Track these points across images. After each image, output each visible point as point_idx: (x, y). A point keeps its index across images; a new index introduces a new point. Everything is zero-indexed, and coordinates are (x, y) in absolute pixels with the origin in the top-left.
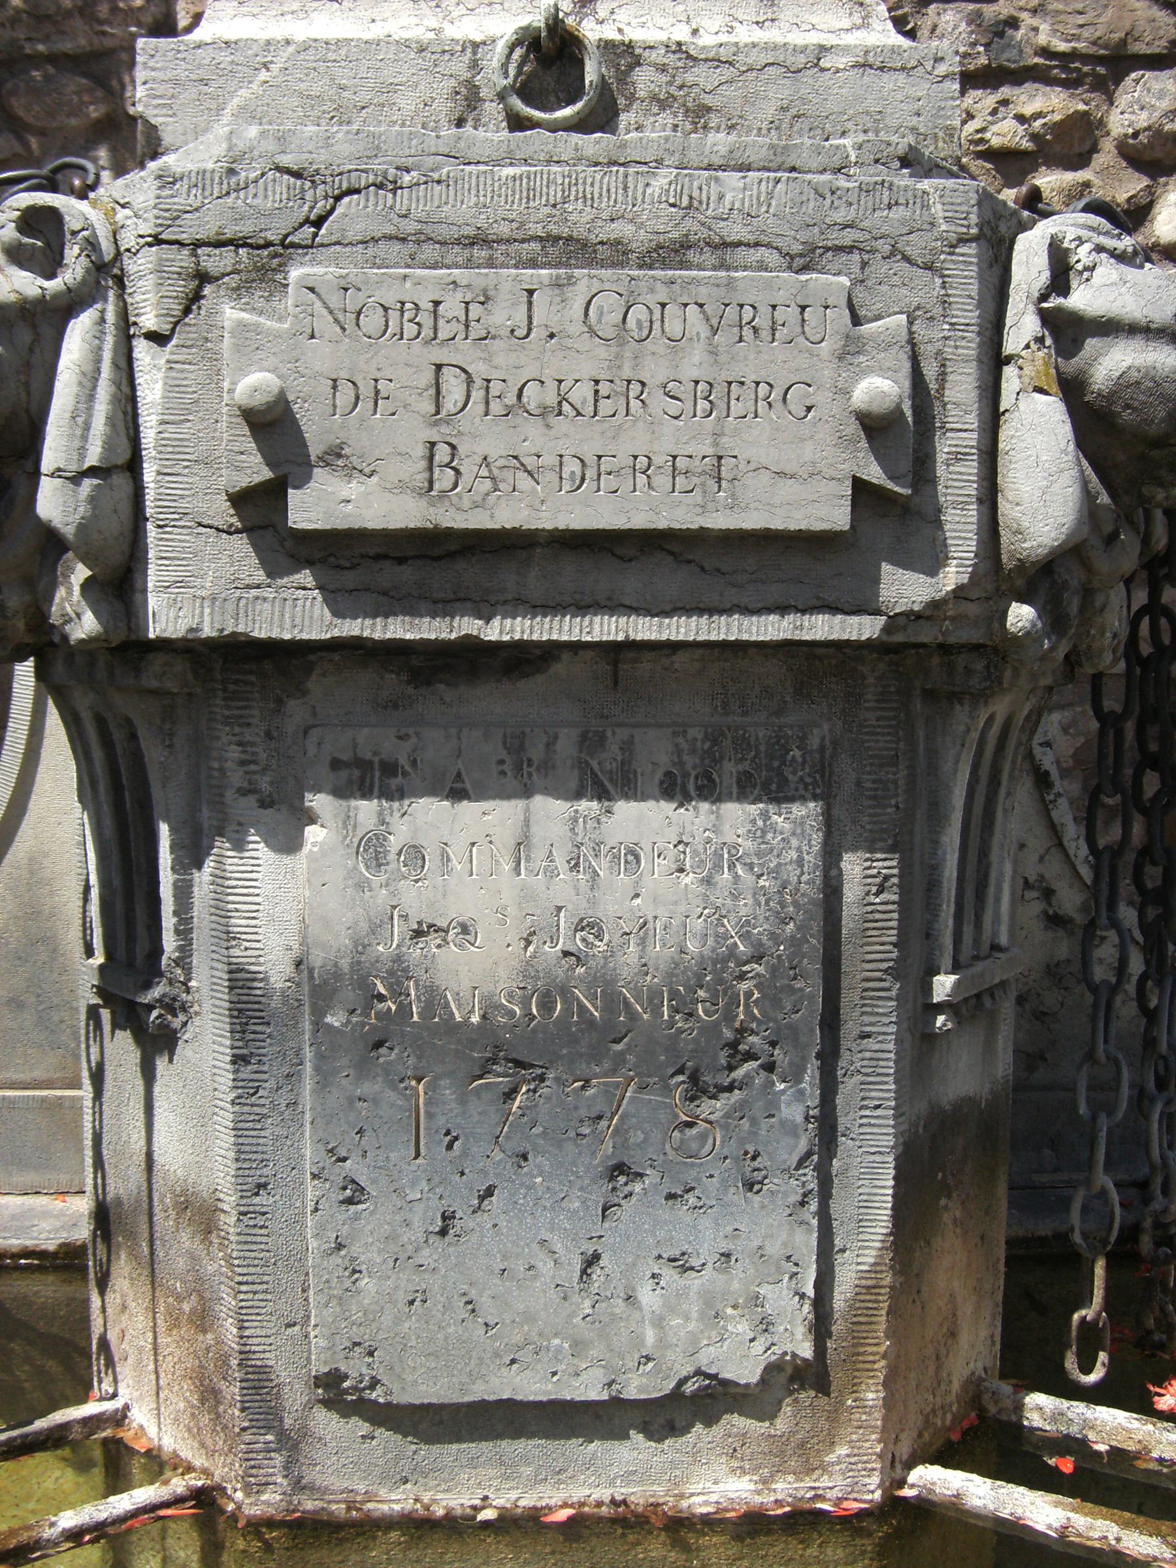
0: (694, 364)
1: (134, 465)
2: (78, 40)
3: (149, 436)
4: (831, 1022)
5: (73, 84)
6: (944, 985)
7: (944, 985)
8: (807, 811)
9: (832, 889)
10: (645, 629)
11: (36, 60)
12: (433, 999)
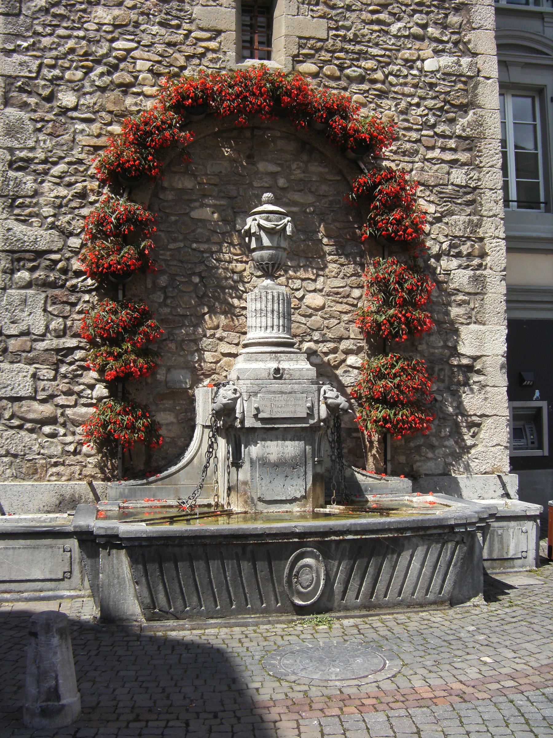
0: (293, 403)
1: (244, 412)
2: (193, 337)
3: (245, 409)
4: (306, 462)
5: (192, 344)
6: (316, 459)
7: (316, 459)
8: (303, 442)
9: (305, 449)
10: (289, 426)
11: (186, 340)
12: (269, 460)
